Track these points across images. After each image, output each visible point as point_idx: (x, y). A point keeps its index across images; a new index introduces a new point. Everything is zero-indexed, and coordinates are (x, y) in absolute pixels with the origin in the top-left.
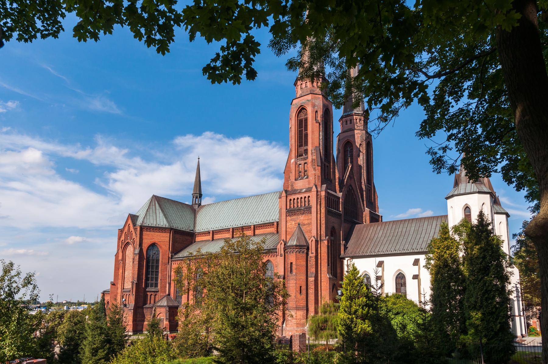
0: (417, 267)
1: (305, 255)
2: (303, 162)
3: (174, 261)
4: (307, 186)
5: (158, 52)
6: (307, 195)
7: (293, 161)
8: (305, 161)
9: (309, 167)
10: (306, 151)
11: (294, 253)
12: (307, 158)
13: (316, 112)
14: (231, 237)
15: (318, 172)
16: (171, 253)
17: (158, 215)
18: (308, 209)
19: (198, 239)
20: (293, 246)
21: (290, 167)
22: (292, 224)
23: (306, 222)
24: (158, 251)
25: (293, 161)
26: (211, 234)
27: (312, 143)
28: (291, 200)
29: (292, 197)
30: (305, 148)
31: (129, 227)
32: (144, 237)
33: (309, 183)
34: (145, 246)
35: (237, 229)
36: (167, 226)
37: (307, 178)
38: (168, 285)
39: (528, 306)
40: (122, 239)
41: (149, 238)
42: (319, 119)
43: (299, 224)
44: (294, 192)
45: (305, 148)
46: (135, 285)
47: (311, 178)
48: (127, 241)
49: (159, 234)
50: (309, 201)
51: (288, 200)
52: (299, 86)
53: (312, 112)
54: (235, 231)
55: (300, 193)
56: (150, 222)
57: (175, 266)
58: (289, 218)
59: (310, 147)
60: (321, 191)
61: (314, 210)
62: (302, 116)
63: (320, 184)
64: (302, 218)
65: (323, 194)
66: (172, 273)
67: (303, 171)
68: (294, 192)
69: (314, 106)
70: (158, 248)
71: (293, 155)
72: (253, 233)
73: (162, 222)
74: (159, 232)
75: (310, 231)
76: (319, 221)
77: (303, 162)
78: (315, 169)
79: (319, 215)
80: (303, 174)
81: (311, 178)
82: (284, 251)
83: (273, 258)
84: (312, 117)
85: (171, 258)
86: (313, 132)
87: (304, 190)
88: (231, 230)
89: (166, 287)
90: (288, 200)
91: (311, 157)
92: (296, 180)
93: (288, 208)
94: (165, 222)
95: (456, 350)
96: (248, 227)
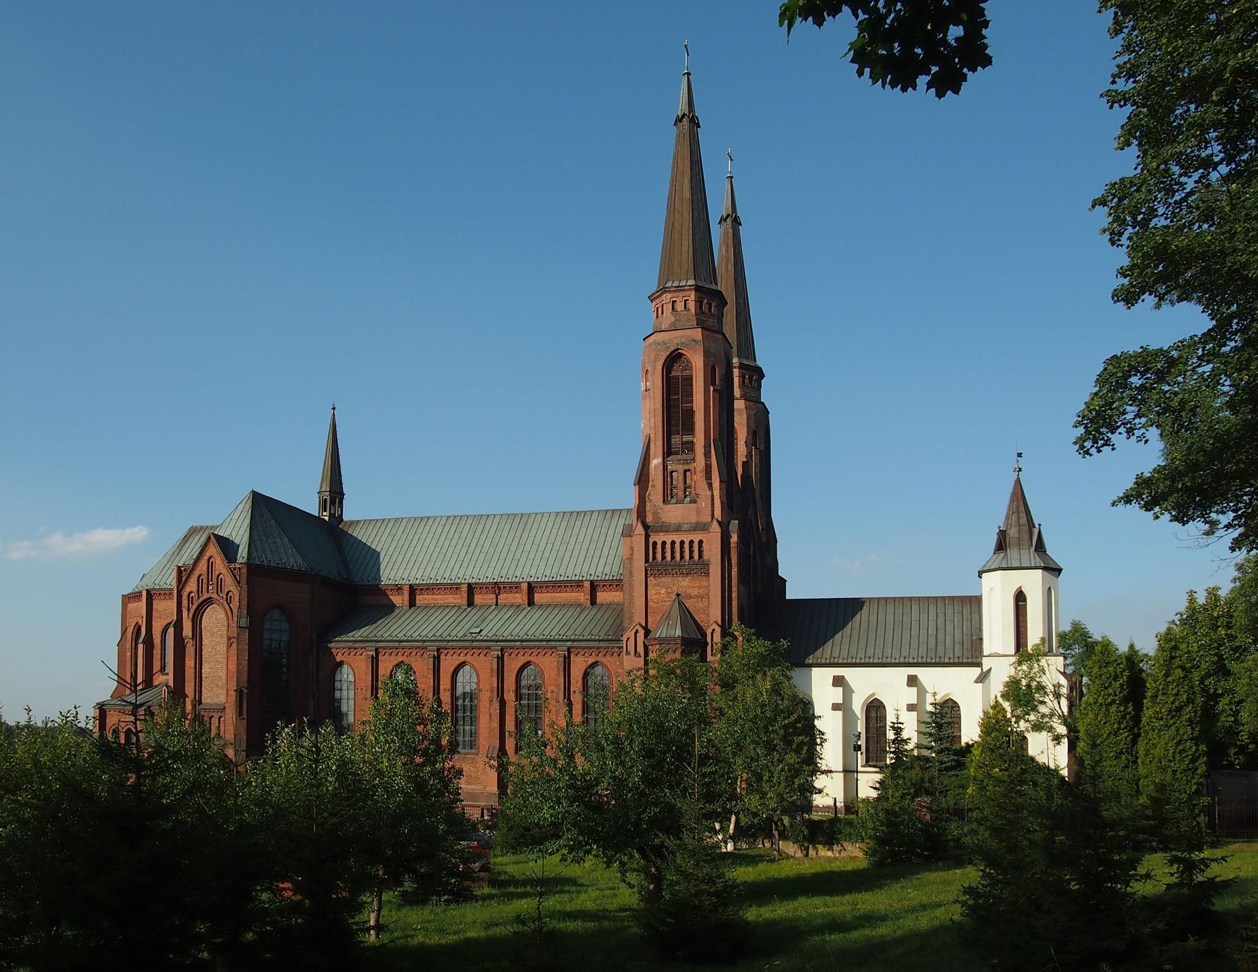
2: (681, 468)
5: (1075, 443)
6: (696, 538)
9: (698, 479)
10: (690, 446)
12: (694, 460)
14: (465, 602)
18: (702, 568)
22: (663, 591)
23: (695, 592)
26: (406, 593)
29: (658, 538)
30: (686, 438)
31: (210, 566)
33: (698, 513)
35: (483, 587)
37: (693, 501)
39: (519, 919)
40: (187, 589)
43: (678, 595)
45: (686, 438)
46: (245, 697)
48: (206, 596)
50: (700, 552)
55: (678, 529)
64: (684, 584)
72: (526, 598)
77: (681, 468)
81: (704, 503)
83: (608, 658)
87: (685, 527)
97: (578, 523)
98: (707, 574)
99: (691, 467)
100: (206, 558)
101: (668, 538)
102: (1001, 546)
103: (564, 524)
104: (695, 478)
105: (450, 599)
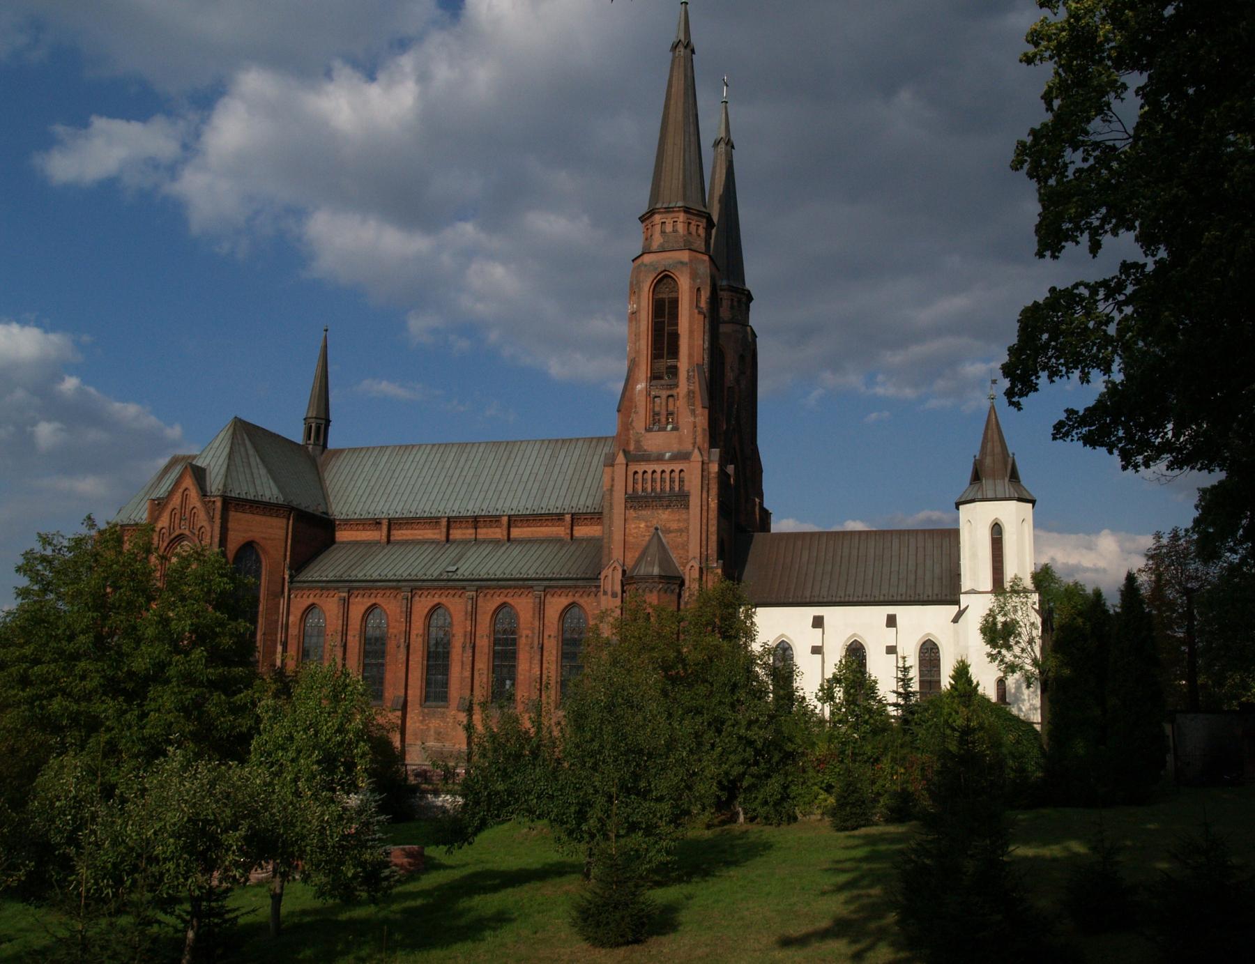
0: (819, 656)
1: (675, 597)
2: (664, 394)
3: (298, 588)
4: (676, 448)
6: (677, 467)
7: (640, 386)
8: (670, 393)
10: (673, 371)
11: (655, 593)
12: (677, 386)
13: (699, 289)
15: (702, 420)
16: (290, 568)
17: (255, 471)
18: (680, 499)
19: (342, 535)
20: (652, 577)
21: (631, 400)
22: (640, 526)
23: (674, 526)
24: (258, 561)
25: (640, 386)
26: (385, 528)
27: (690, 356)
28: (636, 473)
29: (640, 468)
31: (185, 497)
32: (230, 525)
34: (232, 547)
36: (281, 500)
37: (675, 429)
38: (280, 648)
41: (244, 527)
42: (703, 304)
43: (657, 529)
44: (646, 458)
45: (670, 362)
47: (686, 431)
49: (264, 519)
50: (681, 481)
51: (630, 474)
52: (658, 228)
53: (691, 288)
54: (452, 525)
56: (242, 489)
57: (300, 603)
58: (632, 513)
59: (683, 364)
60: (710, 461)
61: (695, 501)
62: (665, 295)
63: (706, 445)
64: (664, 517)
65: (714, 468)
66: (291, 618)
67: (664, 412)
68: (646, 458)
69: (694, 276)
70: (258, 556)
71: (643, 371)
72: (505, 533)
73: (268, 490)
74: (264, 515)
75: (685, 546)
76: (704, 527)
77: (664, 394)
78: (693, 412)
79: (705, 514)
80: (663, 420)
81: (686, 431)
82: (623, 586)
83: (586, 598)
84: (691, 300)
85: (291, 582)
86: (691, 332)
88: (444, 522)
89: (274, 652)
90: (630, 474)
91: (683, 387)
92: (648, 430)
93: (630, 491)
94: (275, 491)
95: (1157, 258)
96: (493, 520)
97: (564, 451)
98: (687, 507)
99: (674, 392)
100: (181, 490)
101: (649, 468)
102: (976, 477)
103: (549, 452)
104: (678, 403)
105: (430, 534)
